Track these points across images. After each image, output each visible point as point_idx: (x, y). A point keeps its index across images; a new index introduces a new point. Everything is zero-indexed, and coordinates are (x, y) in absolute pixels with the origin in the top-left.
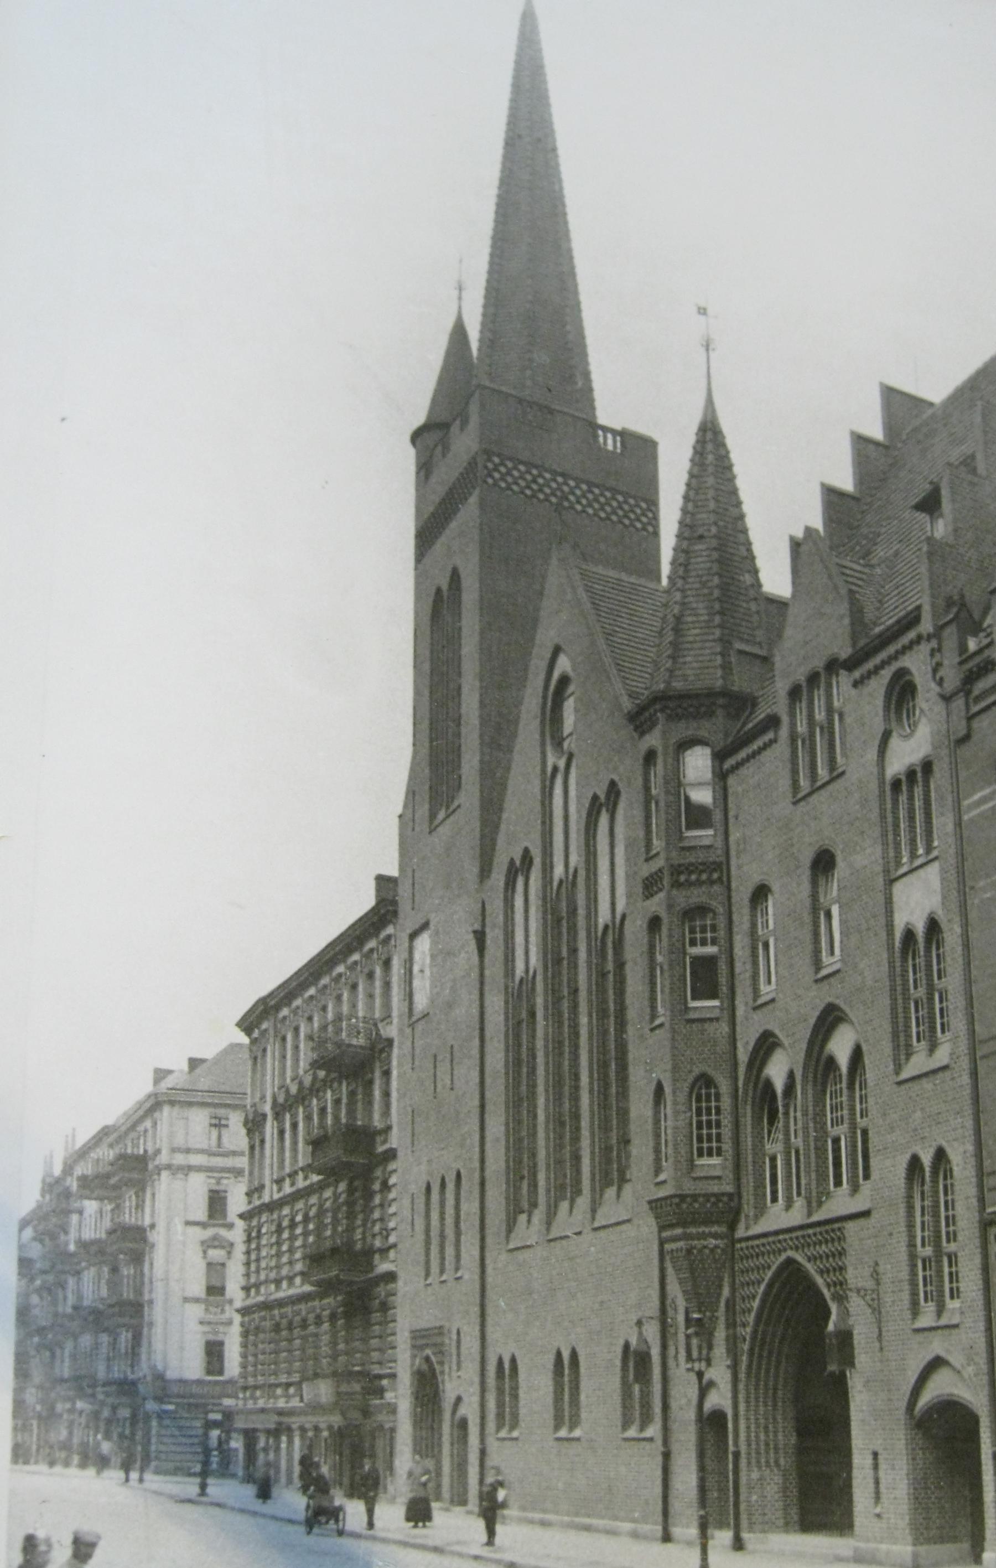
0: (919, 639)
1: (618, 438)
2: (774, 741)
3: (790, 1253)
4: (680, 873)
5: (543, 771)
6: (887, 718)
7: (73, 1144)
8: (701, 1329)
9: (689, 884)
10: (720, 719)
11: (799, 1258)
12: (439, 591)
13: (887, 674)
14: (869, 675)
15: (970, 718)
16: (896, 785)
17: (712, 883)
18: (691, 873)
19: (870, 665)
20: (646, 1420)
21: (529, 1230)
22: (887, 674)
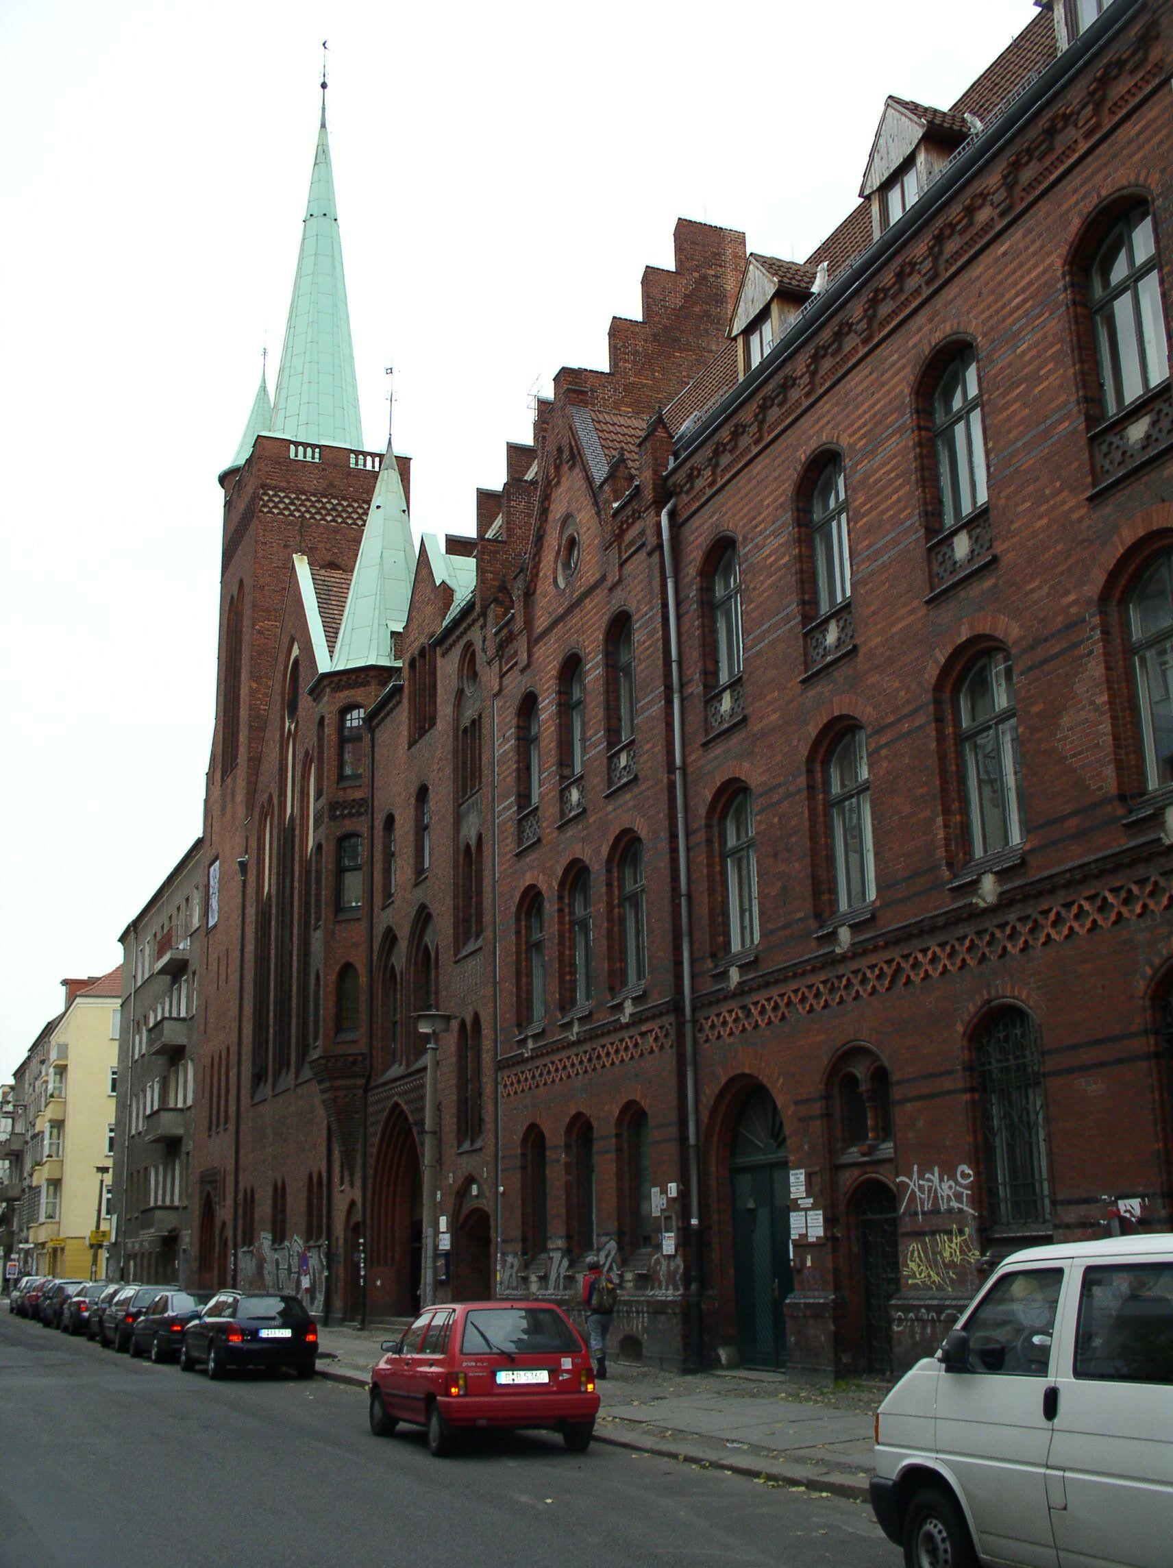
0: (474, 621)
1: (374, 723)
2: (399, 702)
3: (396, 1098)
4: (336, 809)
5: (773, 1126)
6: (460, 677)
7: (1145, 380)
8: (348, 1163)
9: (343, 816)
10: (372, 688)
11: (400, 1101)
12: (232, 597)
13: (462, 643)
14: (451, 646)
15: (501, 677)
16: (465, 730)
17: (361, 815)
18: (345, 808)
19: (450, 641)
20: (319, 1237)
21: (266, 1090)
22: (462, 643)
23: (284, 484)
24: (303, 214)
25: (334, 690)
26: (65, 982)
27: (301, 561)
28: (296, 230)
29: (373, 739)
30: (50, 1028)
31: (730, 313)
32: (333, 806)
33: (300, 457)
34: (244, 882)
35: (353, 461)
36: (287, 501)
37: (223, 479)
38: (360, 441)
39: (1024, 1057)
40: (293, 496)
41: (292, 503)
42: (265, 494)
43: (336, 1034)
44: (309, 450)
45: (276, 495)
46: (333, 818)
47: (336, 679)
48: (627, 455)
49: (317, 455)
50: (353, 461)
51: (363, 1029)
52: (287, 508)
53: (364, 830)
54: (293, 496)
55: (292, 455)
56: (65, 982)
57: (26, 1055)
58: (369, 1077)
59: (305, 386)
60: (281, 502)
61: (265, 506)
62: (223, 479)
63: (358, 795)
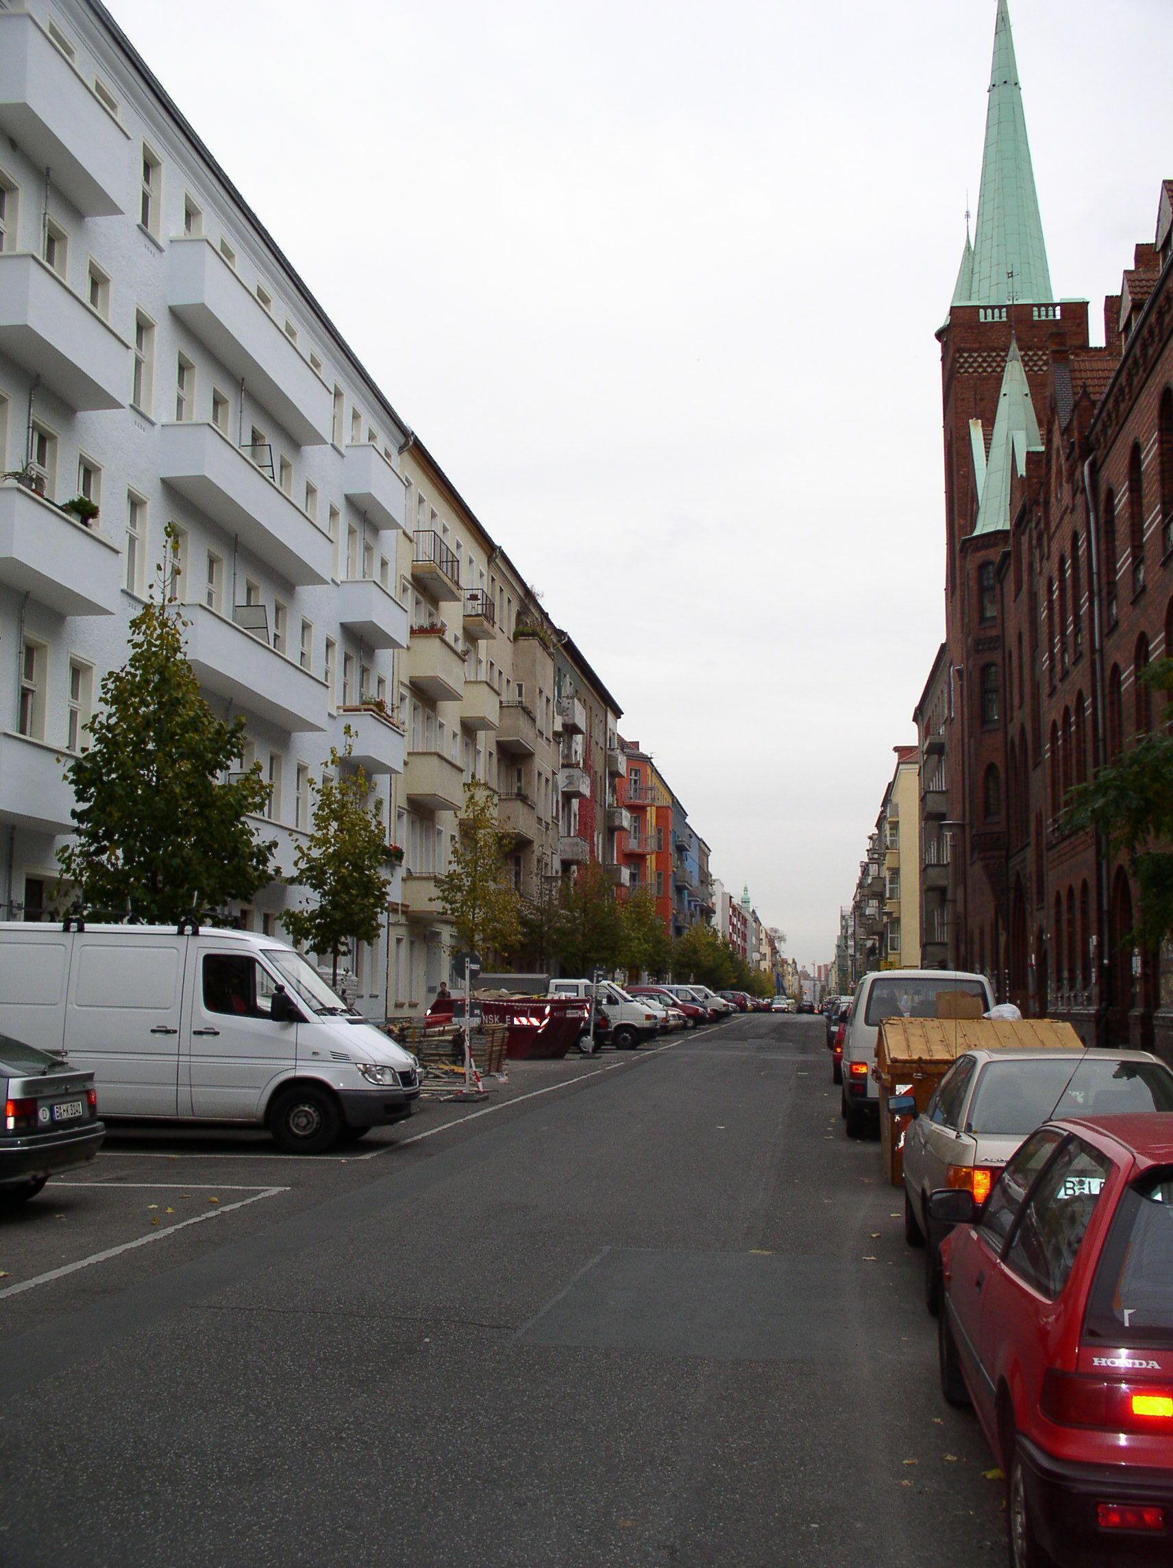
23: (976, 345)
24: (988, 84)
25: (974, 551)
26: (896, 749)
27: (976, 424)
28: (986, 96)
29: (1002, 589)
30: (891, 786)
31: (253, 814)
32: (977, 642)
33: (990, 319)
34: (962, 686)
35: (1036, 313)
36: (980, 360)
37: (939, 335)
38: (1048, 290)
39: (472, 1015)
40: (985, 354)
41: (984, 361)
42: (961, 356)
43: (986, 817)
44: (996, 311)
45: (970, 356)
46: (977, 651)
47: (974, 542)
48: (1090, 389)
49: (1004, 314)
50: (1036, 313)
51: (1003, 813)
52: (980, 366)
53: (999, 661)
54: (985, 354)
55: (982, 320)
56: (896, 749)
57: (880, 809)
58: (1008, 850)
59: (995, 249)
60: (975, 361)
61: (961, 367)
62: (939, 335)
63: (994, 633)
